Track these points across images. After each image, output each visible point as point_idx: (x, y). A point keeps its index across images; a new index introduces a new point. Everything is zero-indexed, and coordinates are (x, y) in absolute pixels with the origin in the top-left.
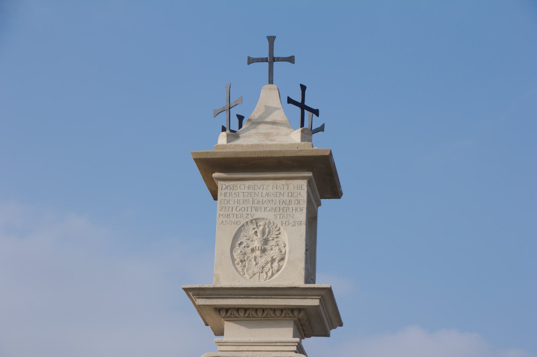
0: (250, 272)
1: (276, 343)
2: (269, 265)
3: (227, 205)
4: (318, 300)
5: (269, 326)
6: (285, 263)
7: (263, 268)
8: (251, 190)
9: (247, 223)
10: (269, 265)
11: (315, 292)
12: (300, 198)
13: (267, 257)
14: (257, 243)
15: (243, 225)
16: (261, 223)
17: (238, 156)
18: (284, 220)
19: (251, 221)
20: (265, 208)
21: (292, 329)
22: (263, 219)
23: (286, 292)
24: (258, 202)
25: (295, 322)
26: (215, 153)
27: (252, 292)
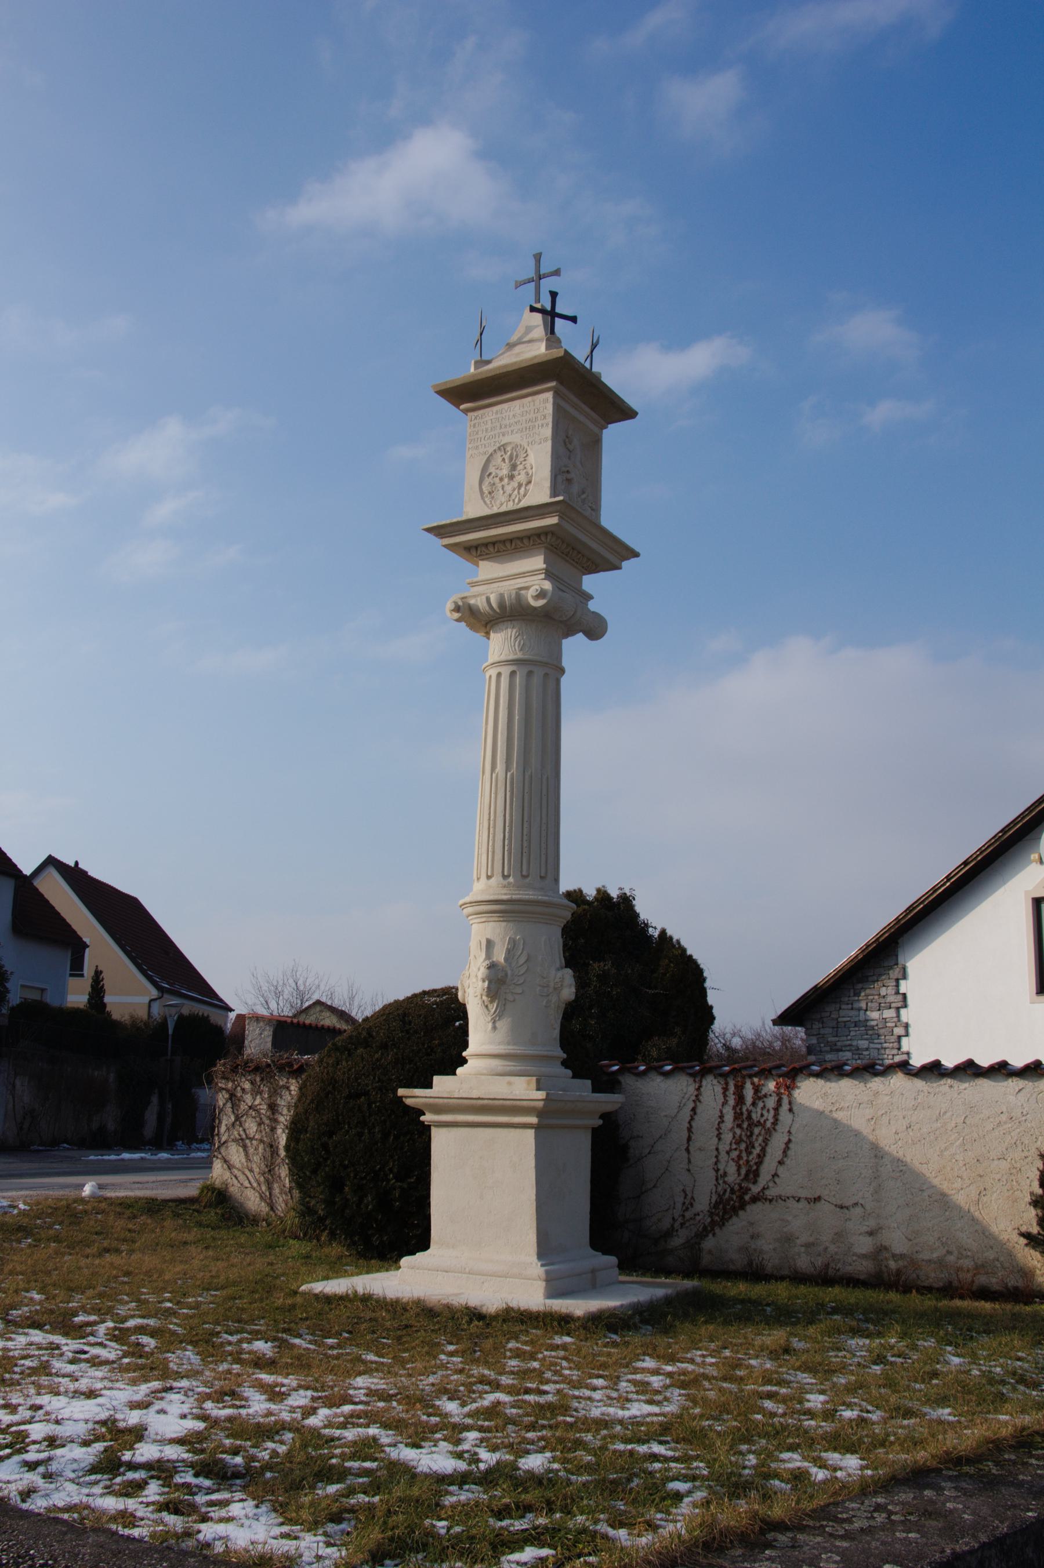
0: (498, 502)
1: (524, 573)
2: (516, 492)
3: (476, 437)
4: (557, 518)
5: (520, 558)
6: (531, 487)
7: (510, 496)
8: (499, 415)
9: (495, 451)
10: (516, 492)
11: (551, 509)
12: (546, 412)
13: (515, 484)
14: (505, 472)
15: (491, 455)
16: (509, 448)
17: (476, 379)
18: (530, 440)
19: (499, 448)
20: (512, 431)
21: (543, 557)
22: (510, 443)
23: (523, 515)
24: (506, 426)
25: (546, 548)
26: (453, 381)
27: (490, 522)
